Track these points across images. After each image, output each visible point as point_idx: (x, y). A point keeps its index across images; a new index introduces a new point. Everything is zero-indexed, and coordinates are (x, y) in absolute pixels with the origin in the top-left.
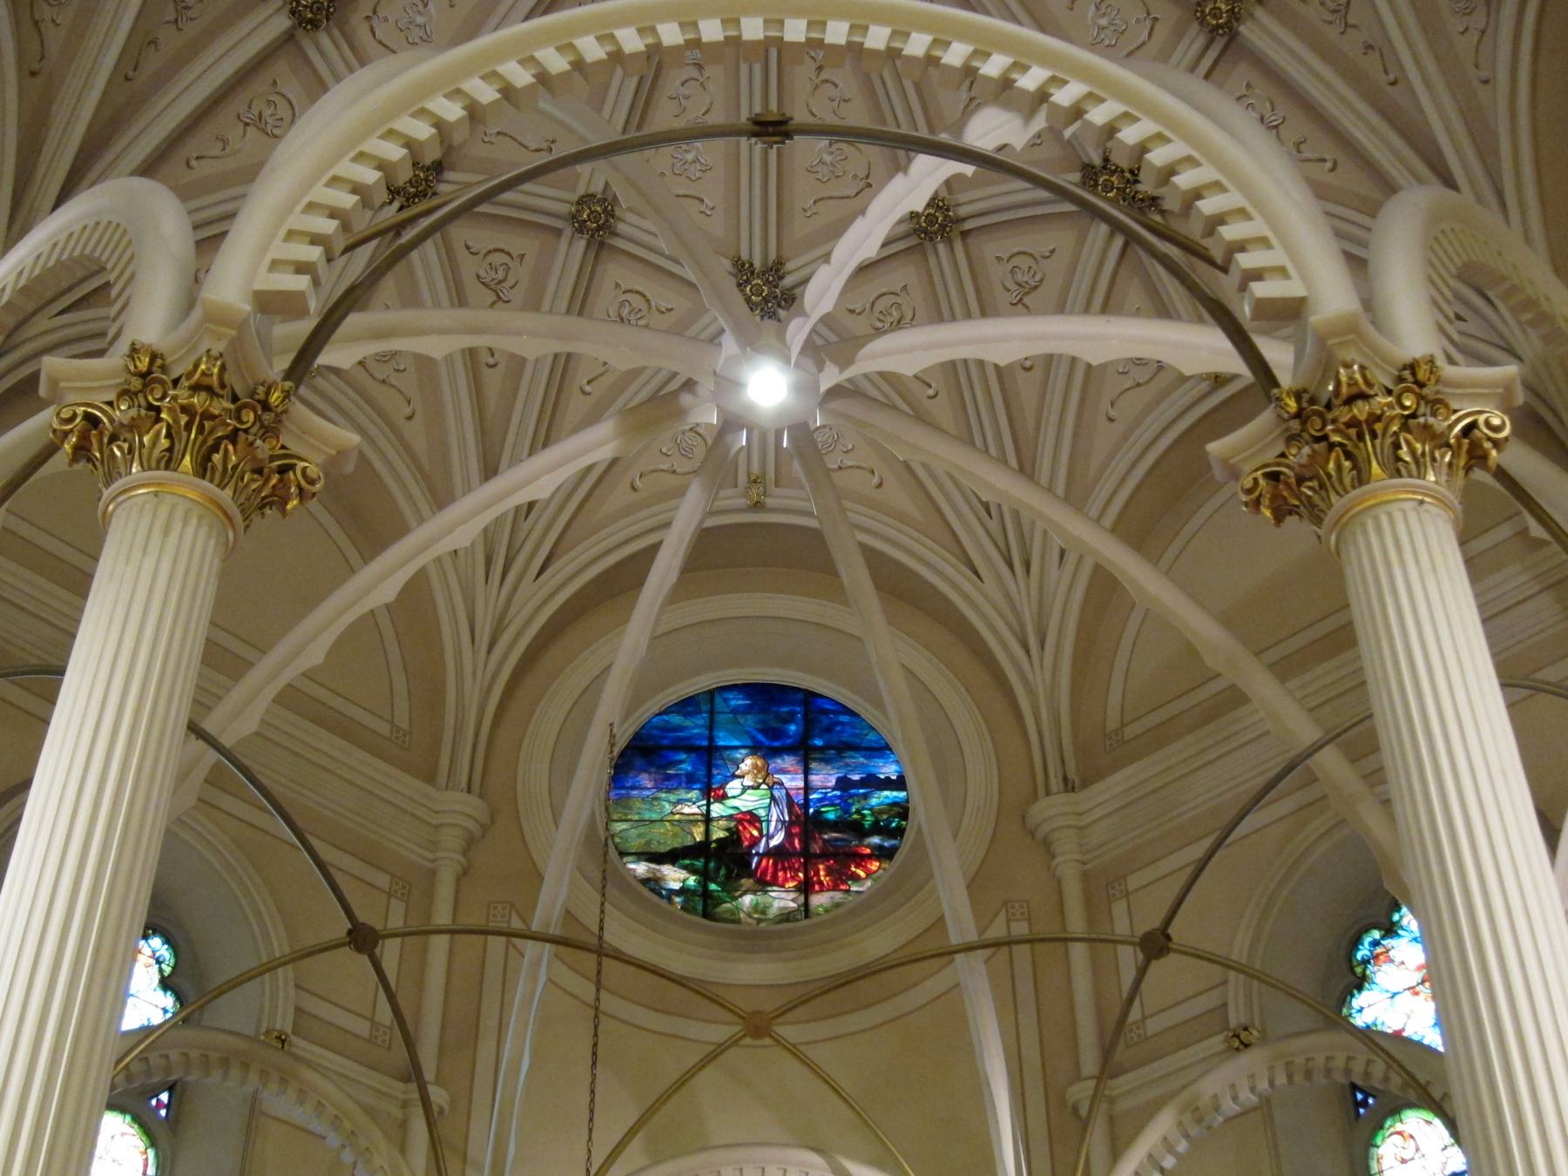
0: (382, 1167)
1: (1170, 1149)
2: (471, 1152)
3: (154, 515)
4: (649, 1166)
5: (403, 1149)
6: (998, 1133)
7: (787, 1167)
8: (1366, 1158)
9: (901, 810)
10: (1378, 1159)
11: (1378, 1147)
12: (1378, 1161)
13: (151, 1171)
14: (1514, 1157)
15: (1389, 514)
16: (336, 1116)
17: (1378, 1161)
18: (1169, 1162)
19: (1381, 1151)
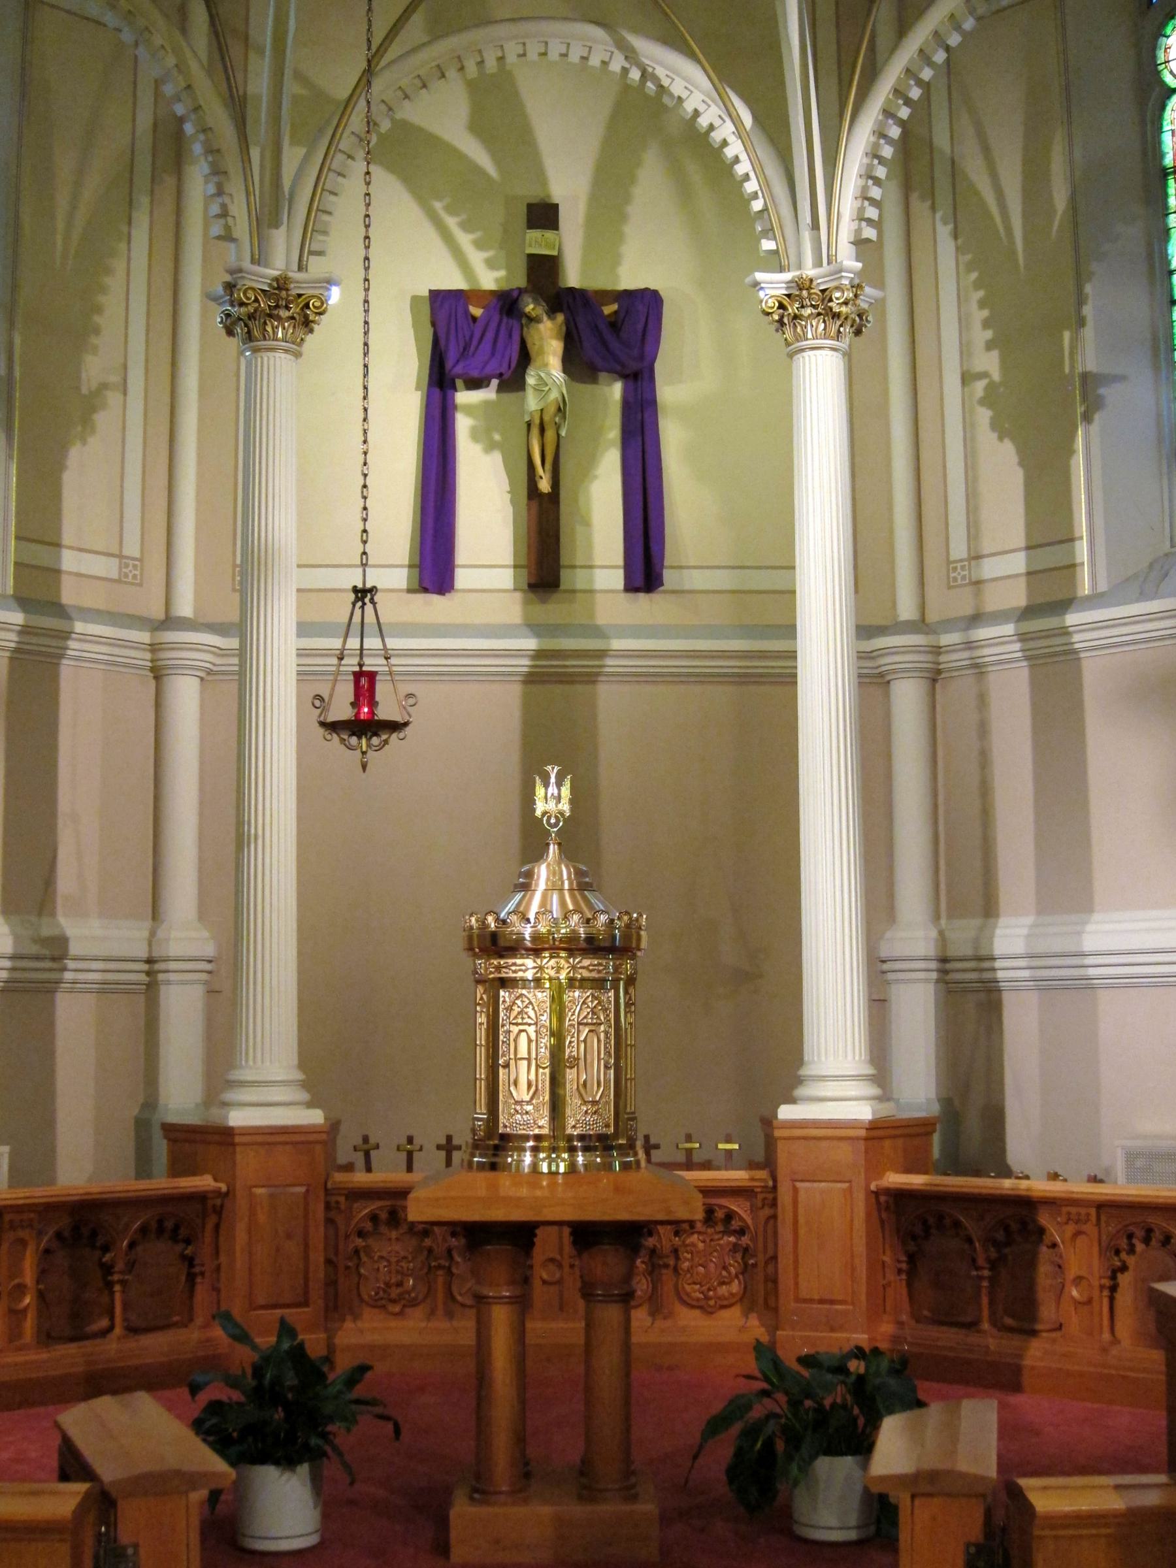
0: (163, 46)
1: (958, 28)
2: (252, 33)
3: (927, 662)
4: (430, 42)
5: (184, 31)
6: (785, 14)
7: (549, 40)
8: (1154, 48)
9: (816, 1405)
10: (1166, 49)
11: (1168, 37)
12: (1165, 51)
13: (777, 3)
14: (801, 81)
15: (262, 358)
16: (130, 12)
17: (1165, 51)
18: (954, 40)
19: (1170, 41)
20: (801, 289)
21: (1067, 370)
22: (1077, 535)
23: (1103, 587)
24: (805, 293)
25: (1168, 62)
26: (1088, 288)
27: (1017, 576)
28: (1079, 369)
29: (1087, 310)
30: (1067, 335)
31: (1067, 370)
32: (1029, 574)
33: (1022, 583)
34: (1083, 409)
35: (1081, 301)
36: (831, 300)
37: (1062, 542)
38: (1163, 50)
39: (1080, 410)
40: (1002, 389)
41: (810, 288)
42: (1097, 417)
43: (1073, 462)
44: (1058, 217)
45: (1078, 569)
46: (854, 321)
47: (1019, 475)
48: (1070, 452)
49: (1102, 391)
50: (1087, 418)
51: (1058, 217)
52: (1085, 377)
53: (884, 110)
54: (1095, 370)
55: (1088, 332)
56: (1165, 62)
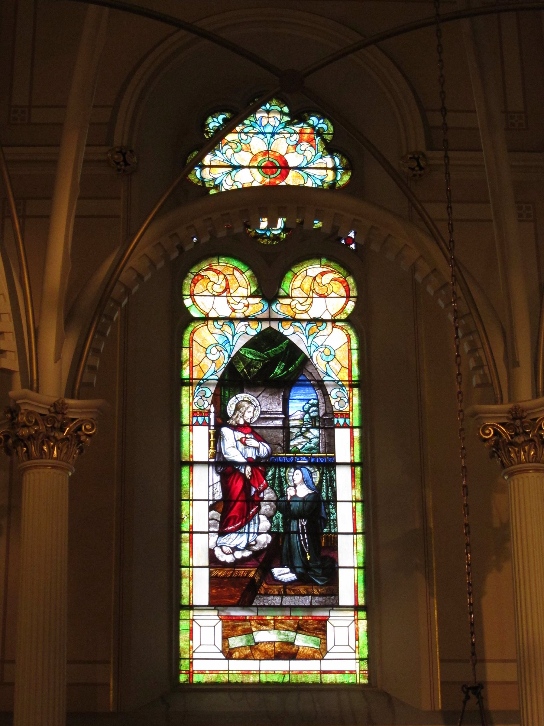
20: (514, 419)
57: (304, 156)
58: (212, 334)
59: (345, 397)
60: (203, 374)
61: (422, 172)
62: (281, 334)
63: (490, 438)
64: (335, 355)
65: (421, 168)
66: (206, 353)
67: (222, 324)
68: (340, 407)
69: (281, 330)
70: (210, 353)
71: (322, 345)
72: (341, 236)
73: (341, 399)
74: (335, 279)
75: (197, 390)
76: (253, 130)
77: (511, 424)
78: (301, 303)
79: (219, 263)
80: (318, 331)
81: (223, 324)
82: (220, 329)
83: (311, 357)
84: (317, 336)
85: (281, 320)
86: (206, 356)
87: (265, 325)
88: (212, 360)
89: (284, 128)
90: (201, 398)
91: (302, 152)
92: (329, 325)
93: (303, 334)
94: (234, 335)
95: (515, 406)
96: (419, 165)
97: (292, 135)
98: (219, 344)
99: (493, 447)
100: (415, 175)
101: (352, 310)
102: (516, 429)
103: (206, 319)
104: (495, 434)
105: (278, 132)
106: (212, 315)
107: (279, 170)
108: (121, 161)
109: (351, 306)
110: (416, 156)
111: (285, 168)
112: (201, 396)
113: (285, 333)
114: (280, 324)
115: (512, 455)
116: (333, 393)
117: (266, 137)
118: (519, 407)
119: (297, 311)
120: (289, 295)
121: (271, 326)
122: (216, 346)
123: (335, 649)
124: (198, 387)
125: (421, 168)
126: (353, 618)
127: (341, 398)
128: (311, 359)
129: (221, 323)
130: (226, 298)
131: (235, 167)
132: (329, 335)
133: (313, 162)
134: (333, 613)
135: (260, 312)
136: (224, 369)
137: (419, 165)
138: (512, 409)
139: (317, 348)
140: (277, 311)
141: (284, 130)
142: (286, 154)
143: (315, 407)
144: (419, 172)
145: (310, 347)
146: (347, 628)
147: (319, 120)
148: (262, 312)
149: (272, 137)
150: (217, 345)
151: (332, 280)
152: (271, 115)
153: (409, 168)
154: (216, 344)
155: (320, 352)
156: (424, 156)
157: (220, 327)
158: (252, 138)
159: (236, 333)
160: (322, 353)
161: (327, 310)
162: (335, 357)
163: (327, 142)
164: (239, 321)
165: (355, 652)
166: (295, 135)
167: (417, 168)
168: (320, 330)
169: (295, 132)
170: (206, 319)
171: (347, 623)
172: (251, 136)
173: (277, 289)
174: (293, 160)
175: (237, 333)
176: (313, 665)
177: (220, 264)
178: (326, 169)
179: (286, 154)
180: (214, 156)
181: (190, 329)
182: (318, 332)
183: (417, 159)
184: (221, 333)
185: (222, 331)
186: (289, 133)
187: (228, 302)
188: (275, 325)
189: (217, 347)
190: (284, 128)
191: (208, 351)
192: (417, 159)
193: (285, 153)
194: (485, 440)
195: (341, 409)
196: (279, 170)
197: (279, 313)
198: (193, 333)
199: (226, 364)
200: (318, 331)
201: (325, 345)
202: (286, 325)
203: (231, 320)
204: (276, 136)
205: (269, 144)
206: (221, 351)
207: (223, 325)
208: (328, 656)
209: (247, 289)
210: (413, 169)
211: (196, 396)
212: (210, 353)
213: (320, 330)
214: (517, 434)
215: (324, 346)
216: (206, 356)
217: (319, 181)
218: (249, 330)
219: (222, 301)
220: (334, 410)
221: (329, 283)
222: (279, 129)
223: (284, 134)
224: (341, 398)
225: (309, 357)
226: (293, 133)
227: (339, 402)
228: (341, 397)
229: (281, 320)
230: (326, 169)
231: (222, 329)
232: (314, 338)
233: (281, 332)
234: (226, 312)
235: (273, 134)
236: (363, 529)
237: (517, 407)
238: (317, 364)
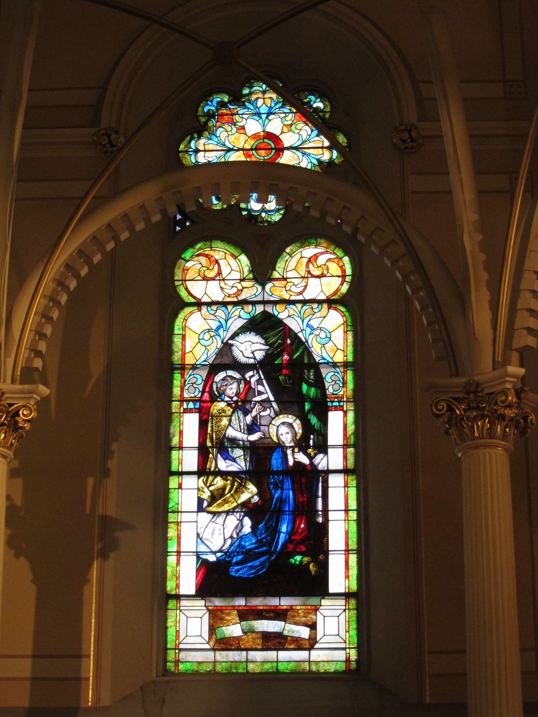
10: (184, 270)
20: (468, 393)
21: (88, 510)
22: (84, 652)
23: (106, 701)
24: (472, 396)
25: (185, 280)
26: (115, 446)
27: (24, 679)
28: (100, 512)
29: (112, 464)
30: (90, 482)
31: (88, 510)
32: (33, 679)
33: (26, 686)
34: (100, 546)
35: (107, 454)
36: (496, 404)
37: (70, 656)
38: (181, 270)
39: (97, 547)
40: (22, 514)
41: (475, 392)
42: (113, 555)
43: (86, 589)
44: (93, 381)
45: (83, 682)
46: (519, 422)
47: (32, 590)
48: (85, 580)
49: (119, 534)
50: (104, 555)
51: (93, 381)
52: (105, 520)
53: (67, 264)
54: (114, 516)
55: (111, 483)
56: (182, 280)
57: (299, 135)
58: (205, 319)
59: (340, 381)
60: (195, 361)
61: (414, 144)
62: (276, 317)
63: (443, 414)
64: (330, 338)
65: (413, 141)
66: (199, 339)
67: (215, 309)
68: (334, 391)
69: (276, 313)
70: (203, 339)
71: (318, 328)
72: (175, 215)
73: (335, 383)
74: (329, 260)
75: (188, 378)
76: (248, 111)
77: (464, 398)
78: (296, 285)
79: (211, 248)
80: (313, 313)
81: (217, 309)
82: (214, 314)
83: (307, 341)
84: (313, 318)
85: (275, 303)
86: (199, 342)
87: (260, 309)
88: (205, 346)
89: (281, 107)
90: (192, 386)
91: (298, 131)
92: (325, 306)
93: (299, 317)
94: (228, 320)
95: (469, 381)
96: (411, 137)
97: (287, 114)
98: (212, 329)
99: (446, 423)
100: (406, 148)
101: (519, 300)
102: (470, 403)
103: (199, 304)
104: (448, 410)
105: (273, 112)
106: (205, 299)
107: (274, 151)
108: (408, 138)
109: (345, 288)
110: (409, 128)
111: (280, 150)
112: (192, 384)
113: (281, 316)
114: (274, 306)
115: (466, 430)
116: (328, 375)
117: (261, 118)
118: (474, 380)
119: (291, 293)
120: (283, 276)
121: (265, 309)
122: (209, 331)
123: (325, 639)
124: (191, 371)
125: (413, 141)
126: (344, 608)
127: (336, 382)
128: (306, 343)
129: (214, 308)
130: (218, 281)
131: (297, 148)
132: (324, 317)
133: (309, 140)
134: (324, 602)
135: (254, 296)
136: (215, 355)
137: (411, 137)
138: (466, 383)
139: (312, 330)
140: (271, 294)
141: (280, 110)
142: (281, 134)
143: (432, 408)
144: (411, 144)
145: (305, 330)
146: (337, 618)
147: (316, 98)
148: (256, 296)
149: (267, 118)
150: (210, 330)
151: (327, 261)
152: (266, 96)
153: (401, 140)
154: (209, 329)
155: (316, 335)
156: (416, 128)
157: (213, 312)
158: (248, 120)
159: (229, 318)
160: (317, 335)
161: (322, 291)
162: (330, 340)
163: (323, 119)
164: (233, 305)
165: (345, 642)
166: (291, 115)
167: (409, 141)
168: (315, 313)
169: (290, 111)
170: (199, 304)
171: (338, 613)
172: (246, 118)
173: (270, 271)
174: (288, 140)
175: (230, 318)
176: (302, 655)
177: (213, 249)
178: (205, 151)
179: (281, 134)
180: (209, 140)
181: (181, 316)
182: (313, 315)
183: (409, 132)
184: (215, 318)
185: (216, 316)
186: (284, 113)
187: (222, 288)
188: (269, 309)
189: (209, 332)
190: (281, 107)
191: (201, 337)
192: (409, 132)
193: (280, 133)
194: (438, 416)
195: (335, 393)
196: (274, 151)
197: (273, 295)
198: (185, 320)
199: (219, 349)
200: (313, 313)
201: (320, 328)
202: (280, 307)
203: (224, 304)
204: (271, 117)
205: (264, 126)
206: (213, 336)
207: (216, 311)
208: (317, 646)
209: (240, 273)
210: (404, 141)
211: (188, 384)
212: (203, 339)
213: (315, 313)
214: (470, 409)
215: (319, 329)
216: (199, 342)
217: (315, 160)
218: (243, 314)
219: (214, 285)
220: (328, 393)
221: (324, 264)
222: (274, 110)
223: (279, 114)
224: (336, 382)
225: (304, 341)
226: (289, 113)
227: (333, 385)
228: (336, 381)
229: (275, 303)
230: (322, 148)
231: (215, 315)
232: (309, 320)
233: (276, 315)
234: (219, 297)
235: (269, 114)
236: (322, 509)
237: (471, 382)
238: (312, 347)
